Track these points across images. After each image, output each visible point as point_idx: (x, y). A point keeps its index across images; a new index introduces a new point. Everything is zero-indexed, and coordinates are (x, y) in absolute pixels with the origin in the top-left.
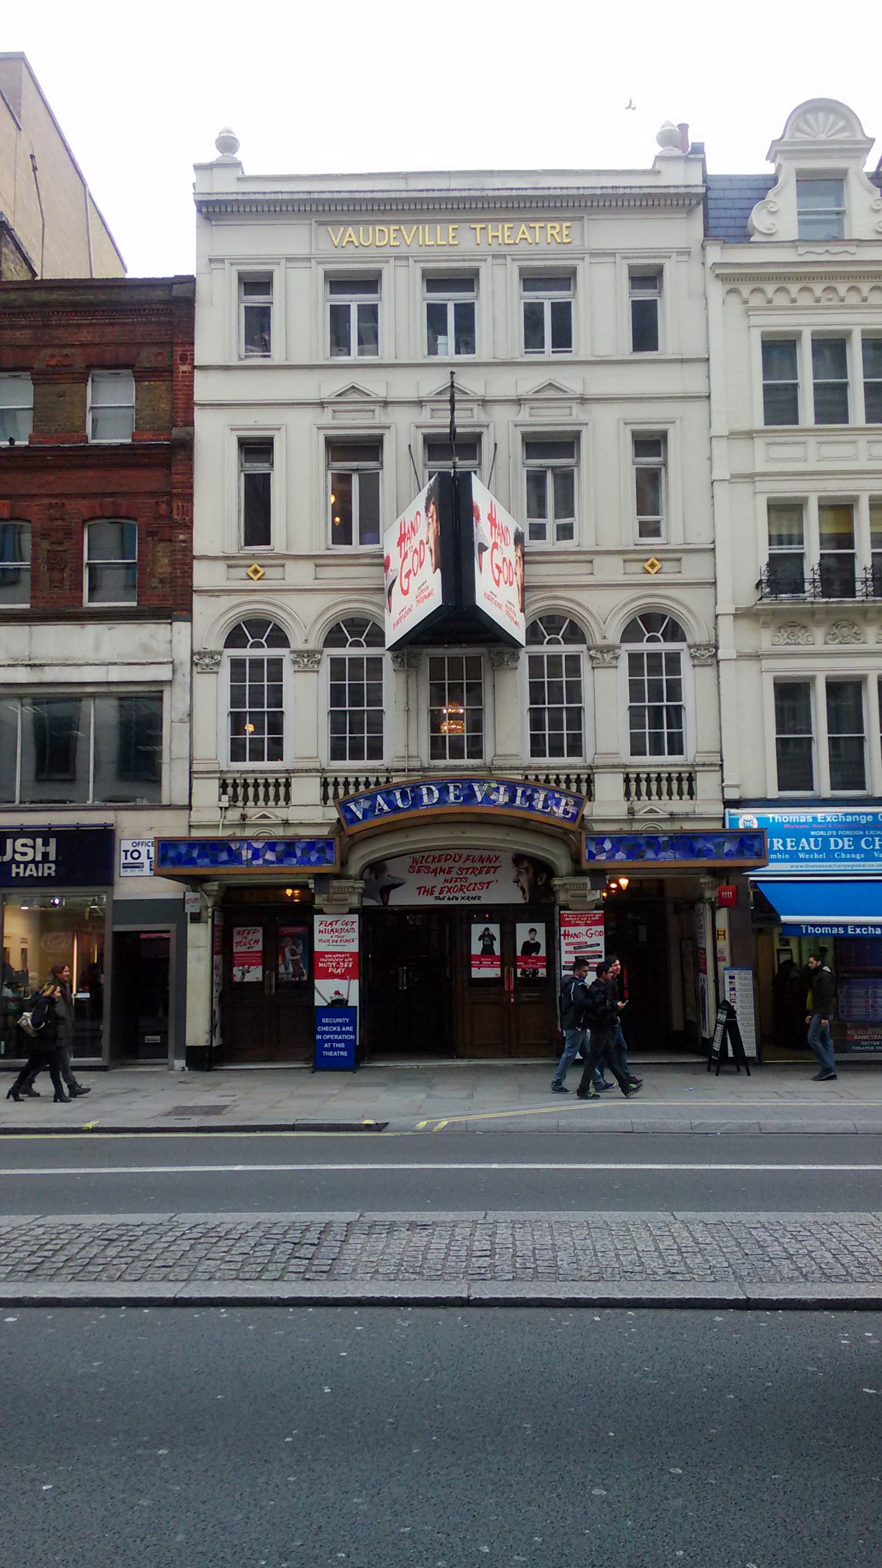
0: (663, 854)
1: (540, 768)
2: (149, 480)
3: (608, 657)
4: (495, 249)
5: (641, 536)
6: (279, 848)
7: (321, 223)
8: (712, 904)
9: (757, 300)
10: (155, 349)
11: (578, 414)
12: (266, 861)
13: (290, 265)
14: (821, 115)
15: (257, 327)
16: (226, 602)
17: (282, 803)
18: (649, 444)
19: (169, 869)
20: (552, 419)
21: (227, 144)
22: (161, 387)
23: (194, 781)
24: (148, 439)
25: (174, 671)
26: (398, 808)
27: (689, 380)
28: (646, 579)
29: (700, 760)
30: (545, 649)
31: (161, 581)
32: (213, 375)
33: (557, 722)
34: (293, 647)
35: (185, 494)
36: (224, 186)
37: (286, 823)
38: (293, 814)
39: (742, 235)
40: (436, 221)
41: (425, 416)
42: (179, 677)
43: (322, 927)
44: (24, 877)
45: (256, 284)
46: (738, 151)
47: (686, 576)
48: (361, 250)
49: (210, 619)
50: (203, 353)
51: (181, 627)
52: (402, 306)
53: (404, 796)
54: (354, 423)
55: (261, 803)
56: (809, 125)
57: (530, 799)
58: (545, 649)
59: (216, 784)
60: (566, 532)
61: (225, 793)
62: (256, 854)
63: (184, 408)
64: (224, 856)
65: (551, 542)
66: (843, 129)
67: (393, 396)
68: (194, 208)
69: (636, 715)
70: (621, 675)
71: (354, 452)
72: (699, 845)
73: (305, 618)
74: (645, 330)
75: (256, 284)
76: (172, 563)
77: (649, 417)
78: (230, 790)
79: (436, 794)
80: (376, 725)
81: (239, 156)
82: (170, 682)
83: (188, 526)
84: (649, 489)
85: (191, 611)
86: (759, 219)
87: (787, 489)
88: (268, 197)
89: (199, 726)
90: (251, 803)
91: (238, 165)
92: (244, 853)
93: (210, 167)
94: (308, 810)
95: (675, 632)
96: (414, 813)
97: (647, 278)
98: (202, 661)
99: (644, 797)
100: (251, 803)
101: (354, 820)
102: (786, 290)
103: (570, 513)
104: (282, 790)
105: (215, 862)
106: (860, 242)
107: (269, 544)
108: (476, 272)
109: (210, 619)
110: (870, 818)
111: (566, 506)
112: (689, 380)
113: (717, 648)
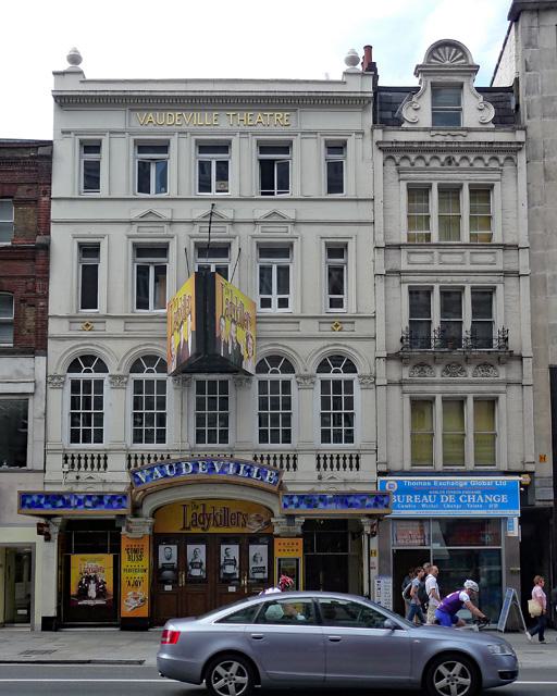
0: (328, 505)
1: (264, 450)
2: (25, 268)
3: (308, 382)
4: (242, 127)
5: (331, 307)
6: (94, 499)
7: (131, 110)
8: (369, 535)
9: (405, 164)
10: (26, 187)
11: (167, 230)
12: (86, 507)
13: (112, 135)
14: (447, 48)
15: (91, 177)
16: (135, 343)
17: (102, 469)
18: (336, 250)
19: (26, 510)
20: (276, 234)
21: (75, 59)
22: (30, 210)
23: (47, 456)
24: (22, 242)
25: (35, 387)
26: (167, 476)
27: (363, 212)
28: (337, 334)
29: (111, 447)
30: (268, 377)
31: (29, 331)
32: (64, 204)
33: (276, 425)
34: (297, 373)
35: (44, 275)
36: (72, 86)
37: (104, 482)
38: (107, 476)
39: (397, 122)
40: (205, 110)
41: (196, 230)
42: (38, 390)
43: (280, 547)
44: (555, 501)
45: (91, 147)
46: (396, 73)
47: (357, 333)
48: (158, 127)
49: (59, 352)
50: (58, 189)
51: (41, 360)
52: (182, 164)
53: (171, 468)
54: (150, 235)
55: (89, 469)
56: (440, 55)
57: (249, 471)
58: (268, 377)
59: (61, 457)
60: (283, 303)
61: (66, 462)
62: (80, 503)
63: (44, 225)
64: (60, 503)
65: (275, 310)
66: (461, 58)
67: (239, 217)
68: (52, 100)
69: (74, 418)
70: (316, 395)
71: (150, 255)
72: (351, 500)
73: (117, 354)
74: (335, 182)
75: (91, 147)
76: (35, 321)
77: (336, 233)
78: (69, 461)
79: (191, 467)
80: (162, 420)
81: (81, 66)
82: (33, 394)
83: (46, 297)
84: (336, 281)
85: (46, 349)
86: (407, 114)
87: (420, 281)
88: (98, 94)
89: (50, 421)
90: (83, 469)
91: (81, 72)
92: (72, 501)
93: (63, 73)
94: (116, 477)
95: (350, 367)
96: (178, 478)
97: (337, 147)
98: (52, 381)
99: (329, 468)
100: (83, 469)
101: (140, 482)
102: (422, 158)
103: (340, 292)
104: (102, 461)
105: (54, 507)
106: (469, 130)
107: (96, 308)
108: (230, 142)
109: (59, 352)
110: (466, 484)
111: (284, 287)
112: (363, 212)
113: (375, 378)
